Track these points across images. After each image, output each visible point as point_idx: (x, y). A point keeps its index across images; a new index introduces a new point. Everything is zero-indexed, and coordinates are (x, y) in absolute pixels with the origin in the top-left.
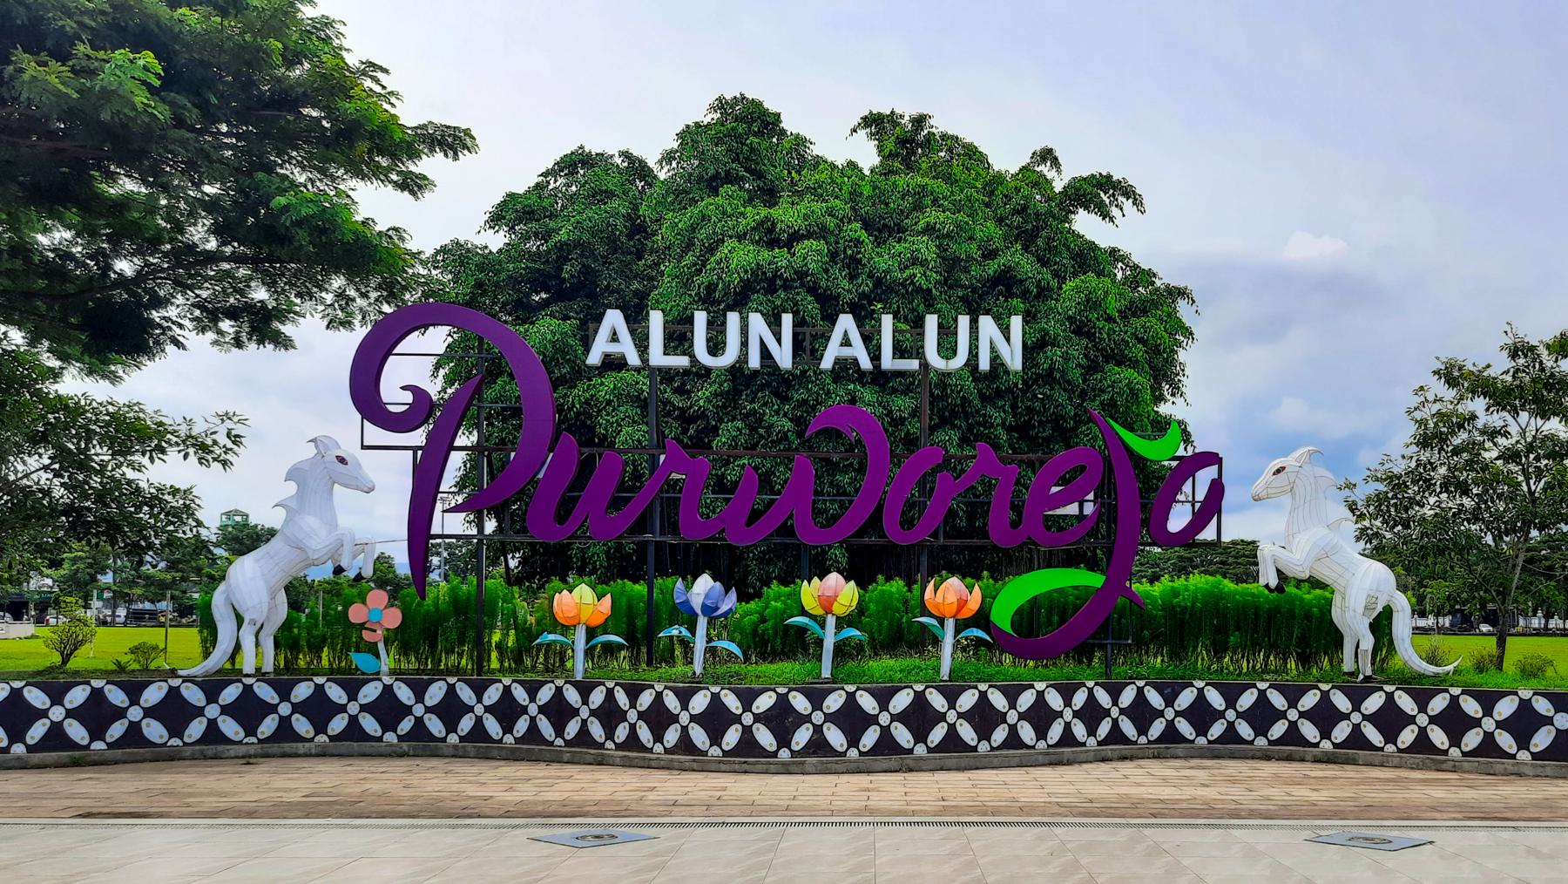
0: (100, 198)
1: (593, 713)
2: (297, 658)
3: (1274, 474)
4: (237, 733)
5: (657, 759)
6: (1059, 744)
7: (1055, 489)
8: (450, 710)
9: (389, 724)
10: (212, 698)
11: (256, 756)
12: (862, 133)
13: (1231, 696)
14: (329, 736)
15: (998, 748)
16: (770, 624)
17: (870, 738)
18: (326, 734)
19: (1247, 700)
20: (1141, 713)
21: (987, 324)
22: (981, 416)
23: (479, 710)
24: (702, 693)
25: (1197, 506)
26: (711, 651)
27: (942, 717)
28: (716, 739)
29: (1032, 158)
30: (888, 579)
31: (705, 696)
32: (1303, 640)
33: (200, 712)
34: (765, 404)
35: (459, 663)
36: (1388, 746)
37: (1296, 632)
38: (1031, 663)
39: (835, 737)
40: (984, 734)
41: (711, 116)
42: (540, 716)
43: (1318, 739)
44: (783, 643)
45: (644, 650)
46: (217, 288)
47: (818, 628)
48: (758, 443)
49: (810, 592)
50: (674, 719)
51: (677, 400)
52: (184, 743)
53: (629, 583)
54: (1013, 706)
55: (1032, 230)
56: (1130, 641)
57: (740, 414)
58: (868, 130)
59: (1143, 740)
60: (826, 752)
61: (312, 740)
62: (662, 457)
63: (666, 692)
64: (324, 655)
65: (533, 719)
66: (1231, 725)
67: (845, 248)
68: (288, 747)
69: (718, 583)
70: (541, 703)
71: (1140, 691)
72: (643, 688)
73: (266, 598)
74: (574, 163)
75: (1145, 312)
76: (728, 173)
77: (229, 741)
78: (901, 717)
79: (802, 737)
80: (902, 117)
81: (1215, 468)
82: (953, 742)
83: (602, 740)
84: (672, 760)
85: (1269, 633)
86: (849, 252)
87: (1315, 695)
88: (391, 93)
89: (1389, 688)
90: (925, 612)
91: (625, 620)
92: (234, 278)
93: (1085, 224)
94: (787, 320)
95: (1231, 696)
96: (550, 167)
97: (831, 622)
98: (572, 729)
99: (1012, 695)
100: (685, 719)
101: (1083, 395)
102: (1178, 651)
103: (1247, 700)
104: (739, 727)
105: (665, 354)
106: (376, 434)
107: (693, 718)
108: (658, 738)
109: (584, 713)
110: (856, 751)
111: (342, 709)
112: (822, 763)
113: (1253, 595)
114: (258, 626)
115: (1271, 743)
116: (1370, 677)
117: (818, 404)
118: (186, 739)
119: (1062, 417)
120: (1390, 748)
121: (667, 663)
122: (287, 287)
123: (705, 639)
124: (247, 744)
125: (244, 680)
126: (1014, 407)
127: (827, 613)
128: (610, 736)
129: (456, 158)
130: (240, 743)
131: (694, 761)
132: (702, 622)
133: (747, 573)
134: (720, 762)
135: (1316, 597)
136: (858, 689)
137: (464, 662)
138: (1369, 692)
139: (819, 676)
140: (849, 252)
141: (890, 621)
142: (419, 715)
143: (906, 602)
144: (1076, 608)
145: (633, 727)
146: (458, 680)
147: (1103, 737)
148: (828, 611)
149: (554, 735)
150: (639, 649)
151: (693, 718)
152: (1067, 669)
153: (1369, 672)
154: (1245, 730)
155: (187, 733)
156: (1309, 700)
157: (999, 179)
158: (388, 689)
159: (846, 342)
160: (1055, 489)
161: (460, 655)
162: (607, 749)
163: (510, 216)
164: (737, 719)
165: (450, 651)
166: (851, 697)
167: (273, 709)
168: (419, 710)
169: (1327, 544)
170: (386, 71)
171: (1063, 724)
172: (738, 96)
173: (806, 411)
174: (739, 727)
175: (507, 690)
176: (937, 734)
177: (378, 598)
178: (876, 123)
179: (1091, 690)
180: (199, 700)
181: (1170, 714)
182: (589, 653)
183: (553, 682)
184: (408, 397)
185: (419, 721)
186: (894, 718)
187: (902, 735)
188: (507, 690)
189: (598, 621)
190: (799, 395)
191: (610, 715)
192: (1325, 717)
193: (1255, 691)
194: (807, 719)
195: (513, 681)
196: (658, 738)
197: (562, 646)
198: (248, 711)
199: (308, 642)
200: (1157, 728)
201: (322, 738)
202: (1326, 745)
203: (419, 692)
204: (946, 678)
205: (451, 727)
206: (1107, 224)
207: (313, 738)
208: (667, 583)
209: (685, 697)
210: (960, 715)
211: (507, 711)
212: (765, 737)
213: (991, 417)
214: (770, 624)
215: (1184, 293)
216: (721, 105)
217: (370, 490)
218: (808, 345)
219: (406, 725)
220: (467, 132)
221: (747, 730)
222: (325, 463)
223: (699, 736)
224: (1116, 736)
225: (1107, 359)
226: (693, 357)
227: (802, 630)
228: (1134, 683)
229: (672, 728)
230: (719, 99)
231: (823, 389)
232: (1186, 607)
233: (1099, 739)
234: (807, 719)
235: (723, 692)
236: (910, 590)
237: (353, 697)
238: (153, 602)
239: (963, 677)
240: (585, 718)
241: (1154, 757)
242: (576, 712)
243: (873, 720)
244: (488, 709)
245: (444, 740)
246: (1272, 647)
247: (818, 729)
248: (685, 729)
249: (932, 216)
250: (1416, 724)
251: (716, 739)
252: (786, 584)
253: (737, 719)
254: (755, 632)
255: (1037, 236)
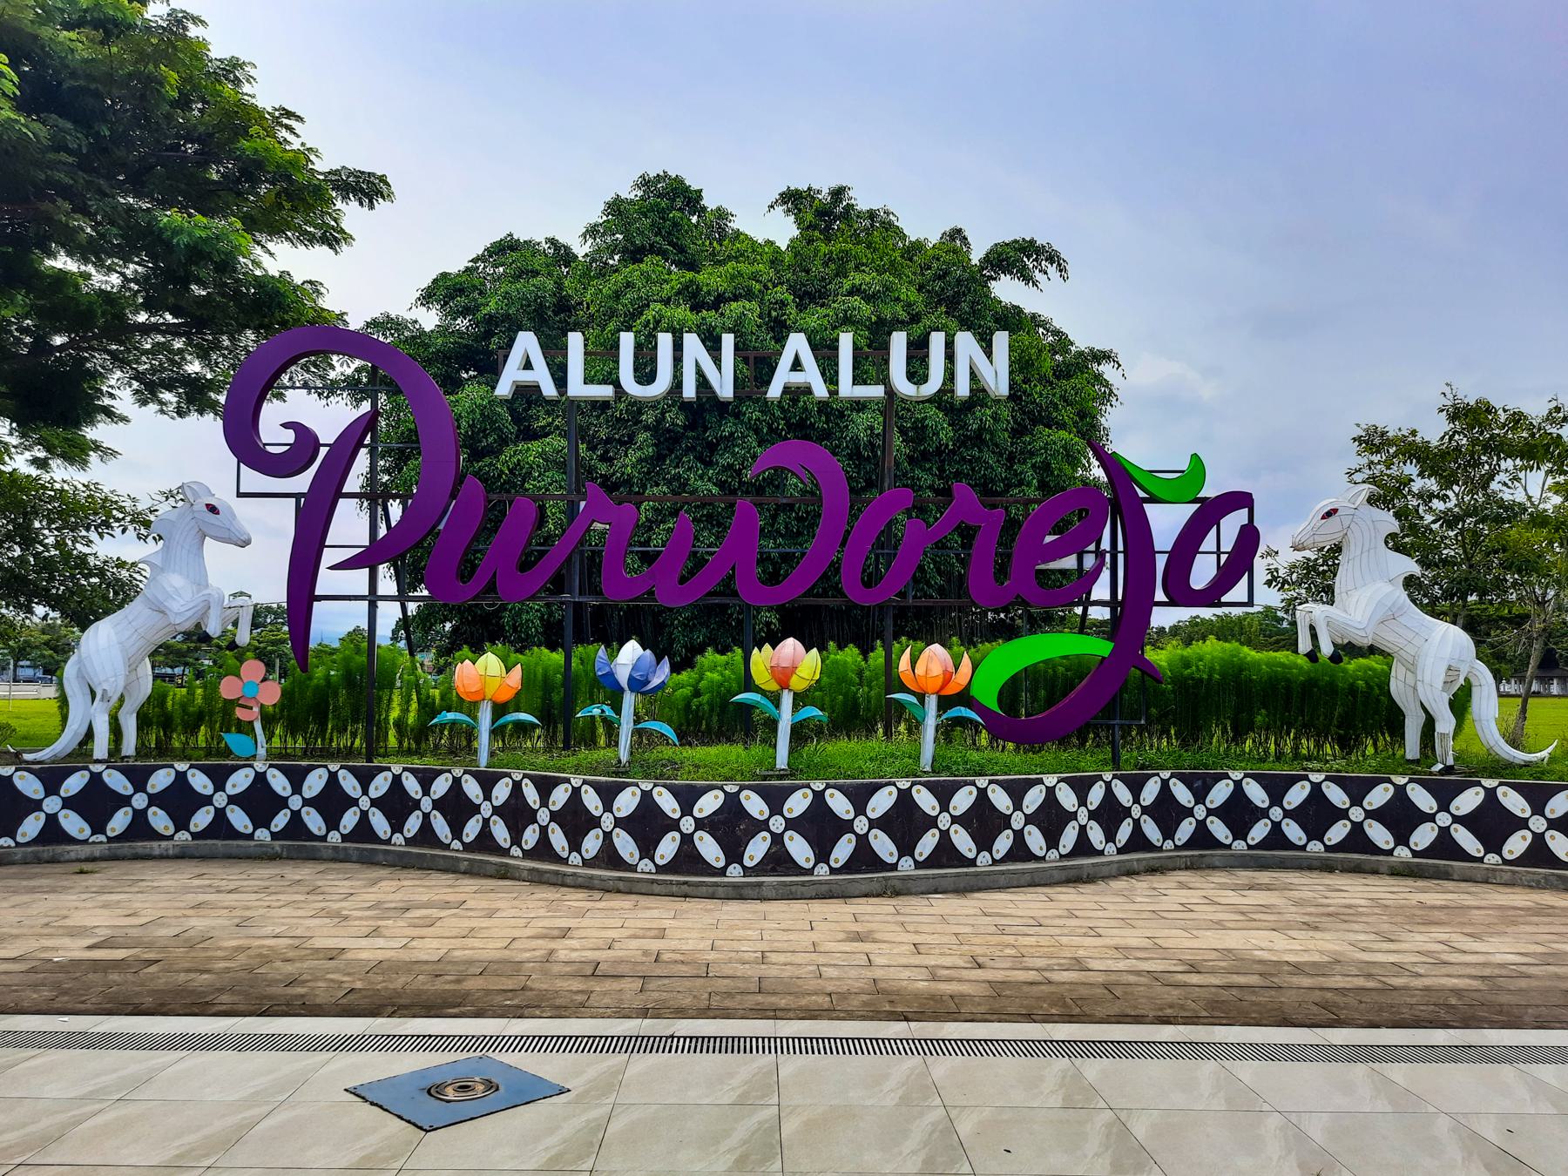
0: (39, 275)
1: (497, 811)
2: (171, 738)
3: (1323, 518)
4: (81, 831)
5: (574, 874)
6: (1073, 854)
7: (1049, 539)
8: (332, 802)
9: (261, 819)
10: (52, 788)
11: (92, 859)
12: (780, 209)
13: (1277, 790)
14: (191, 833)
15: (1003, 860)
16: (705, 698)
17: (843, 850)
18: (188, 830)
19: (1297, 795)
20: (1167, 812)
21: (966, 343)
22: (908, 478)
23: (365, 803)
24: (629, 790)
25: (1224, 558)
26: (638, 733)
27: (932, 822)
28: (647, 850)
29: (941, 238)
30: (841, 647)
31: (634, 794)
32: (1347, 722)
33: (37, 806)
34: (690, 469)
35: (353, 743)
36: (1489, 856)
37: (1339, 710)
38: (1010, 746)
39: (800, 849)
40: (984, 842)
41: (635, 193)
42: (435, 812)
43: (1392, 845)
44: (721, 721)
45: (560, 727)
46: (154, 362)
47: (770, 705)
48: (682, 507)
49: (762, 660)
50: (595, 822)
51: (603, 468)
52: (17, 843)
53: (545, 651)
54: (1018, 806)
55: (953, 296)
56: (1143, 722)
57: (664, 479)
58: (785, 207)
59: (1169, 844)
60: (788, 868)
61: (171, 838)
62: (583, 504)
63: (585, 787)
64: (201, 737)
65: (426, 816)
66: (1276, 826)
67: (770, 312)
68: (141, 846)
69: (648, 651)
70: (436, 797)
71: (1165, 783)
72: (556, 782)
73: (122, 671)
74: (505, 248)
75: (1069, 376)
76: (652, 246)
77: (72, 840)
78: (880, 823)
79: (757, 849)
80: (819, 192)
81: (1245, 511)
82: (946, 853)
83: (507, 845)
84: (592, 877)
85: (1303, 711)
86: (774, 314)
87: (1386, 790)
88: (310, 149)
89: (1489, 783)
90: (904, 689)
91: (540, 694)
92: (171, 351)
93: (1006, 290)
94: (728, 341)
95: (1277, 790)
96: (480, 253)
97: (787, 700)
98: (472, 829)
99: (1017, 792)
100: (608, 823)
101: (1011, 458)
102: (1191, 734)
103: (1297, 795)
104: (677, 835)
105: (585, 383)
106: (254, 480)
107: (619, 822)
108: (575, 846)
109: (486, 809)
110: (826, 868)
111: (207, 800)
112: (784, 884)
113: (1283, 665)
114: (115, 699)
115: (1328, 849)
116: (1451, 767)
117: (744, 468)
118: (20, 839)
119: (992, 480)
120: (1492, 858)
121: (587, 746)
122: (221, 359)
123: (632, 718)
124: (94, 843)
125: (91, 767)
126: (942, 470)
127: (782, 688)
128: (516, 840)
129: (371, 207)
130: (85, 842)
131: (620, 879)
132: (629, 700)
133: (671, 641)
134: (653, 881)
135: (1359, 668)
136: (828, 786)
137: (357, 742)
138: (1460, 788)
139: (773, 767)
140: (774, 314)
141: (845, 695)
142: (295, 808)
143: (860, 673)
144: (1069, 685)
145: (544, 830)
146: (341, 767)
147: (1123, 843)
148: (784, 685)
149: (450, 836)
150: (555, 727)
151: (619, 822)
152: (1088, 764)
153: (1450, 762)
154: (1294, 832)
155: (20, 831)
156: (1379, 796)
157: (918, 246)
158: (260, 778)
159: (797, 365)
160: (1049, 539)
161: (354, 735)
162: (513, 857)
163: (441, 292)
164: (674, 825)
165: (342, 730)
166: (819, 796)
167: (125, 801)
168: (295, 803)
169: (1394, 604)
170: (299, 119)
171: (1077, 828)
172: (662, 174)
173: (731, 476)
174: (677, 835)
175: (397, 780)
176: (927, 844)
177: (253, 669)
178: (793, 200)
179: (1108, 785)
180: (36, 792)
181: (1200, 812)
182: (496, 732)
183: (449, 771)
184: (289, 436)
185: (296, 815)
186: (873, 824)
187: (883, 845)
188: (397, 780)
189: (504, 697)
190: (725, 459)
191: (516, 814)
192: (1401, 818)
193: (1307, 785)
194: (764, 825)
195: (405, 769)
196: (575, 846)
197: (468, 726)
198: (96, 804)
199: (182, 720)
200: (1186, 830)
201: (183, 836)
202: (1403, 853)
203: (297, 778)
204: (928, 769)
205: (332, 823)
206: (1031, 288)
207: (173, 836)
208: (588, 650)
209: (608, 795)
210: (955, 820)
211: (397, 805)
212: (709, 849)
213: (918, 479)
214: (705, 698)
215: (1109, 357)
216: (645, 183)
217: (245, 543)
218: (758, 366)
219: (281, 820)
220: (383, 179)
221: (687, 840)
222: (193, 512)
223: (625, 845)
224: (1138, 841)
225: (1035, 422)
226: (617, 385)
227: (747, 708)
228: (1158, 775)
229: (593, 833)
230: (643, 177)
231: (748, 452)
232: (1201, 680)
233: (1119, 846)
234: (764, 825)
235: (656, 790)
236: (866, 659)
237: (219, 786)
238: (172, 667)
239: (948, 768)
240: (487, 816)
241: (1187, 868)
242: (476, 809)
243: (847, 826)
244: (374, 803)
245: (324, 838)
246: (1306, 729)
247: (777, 839)
248: (608, 836)
249: (856, 278)
250: (1544, 833)
251: (647, 850)
252: (722, 653)
253: (674, 825)
254: (688, 706)
255: (959, 303)
